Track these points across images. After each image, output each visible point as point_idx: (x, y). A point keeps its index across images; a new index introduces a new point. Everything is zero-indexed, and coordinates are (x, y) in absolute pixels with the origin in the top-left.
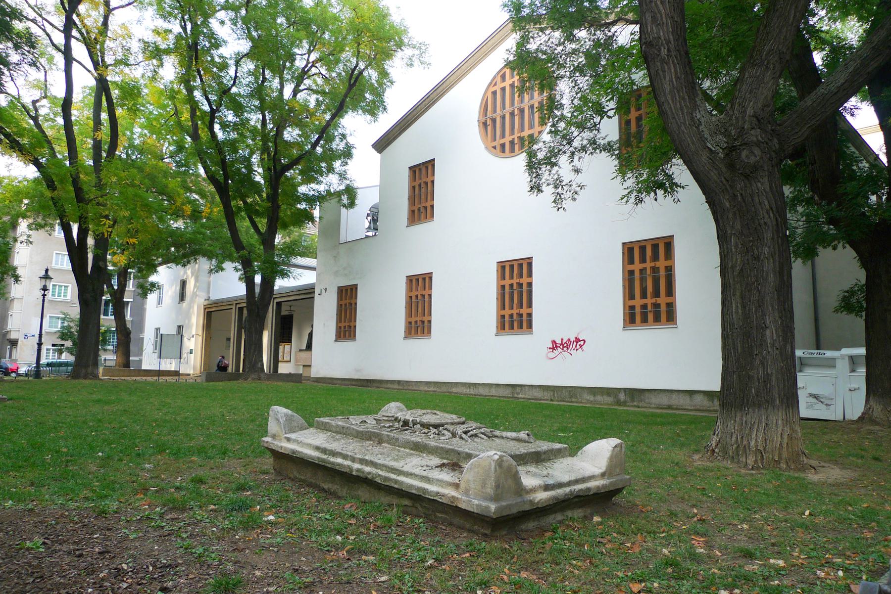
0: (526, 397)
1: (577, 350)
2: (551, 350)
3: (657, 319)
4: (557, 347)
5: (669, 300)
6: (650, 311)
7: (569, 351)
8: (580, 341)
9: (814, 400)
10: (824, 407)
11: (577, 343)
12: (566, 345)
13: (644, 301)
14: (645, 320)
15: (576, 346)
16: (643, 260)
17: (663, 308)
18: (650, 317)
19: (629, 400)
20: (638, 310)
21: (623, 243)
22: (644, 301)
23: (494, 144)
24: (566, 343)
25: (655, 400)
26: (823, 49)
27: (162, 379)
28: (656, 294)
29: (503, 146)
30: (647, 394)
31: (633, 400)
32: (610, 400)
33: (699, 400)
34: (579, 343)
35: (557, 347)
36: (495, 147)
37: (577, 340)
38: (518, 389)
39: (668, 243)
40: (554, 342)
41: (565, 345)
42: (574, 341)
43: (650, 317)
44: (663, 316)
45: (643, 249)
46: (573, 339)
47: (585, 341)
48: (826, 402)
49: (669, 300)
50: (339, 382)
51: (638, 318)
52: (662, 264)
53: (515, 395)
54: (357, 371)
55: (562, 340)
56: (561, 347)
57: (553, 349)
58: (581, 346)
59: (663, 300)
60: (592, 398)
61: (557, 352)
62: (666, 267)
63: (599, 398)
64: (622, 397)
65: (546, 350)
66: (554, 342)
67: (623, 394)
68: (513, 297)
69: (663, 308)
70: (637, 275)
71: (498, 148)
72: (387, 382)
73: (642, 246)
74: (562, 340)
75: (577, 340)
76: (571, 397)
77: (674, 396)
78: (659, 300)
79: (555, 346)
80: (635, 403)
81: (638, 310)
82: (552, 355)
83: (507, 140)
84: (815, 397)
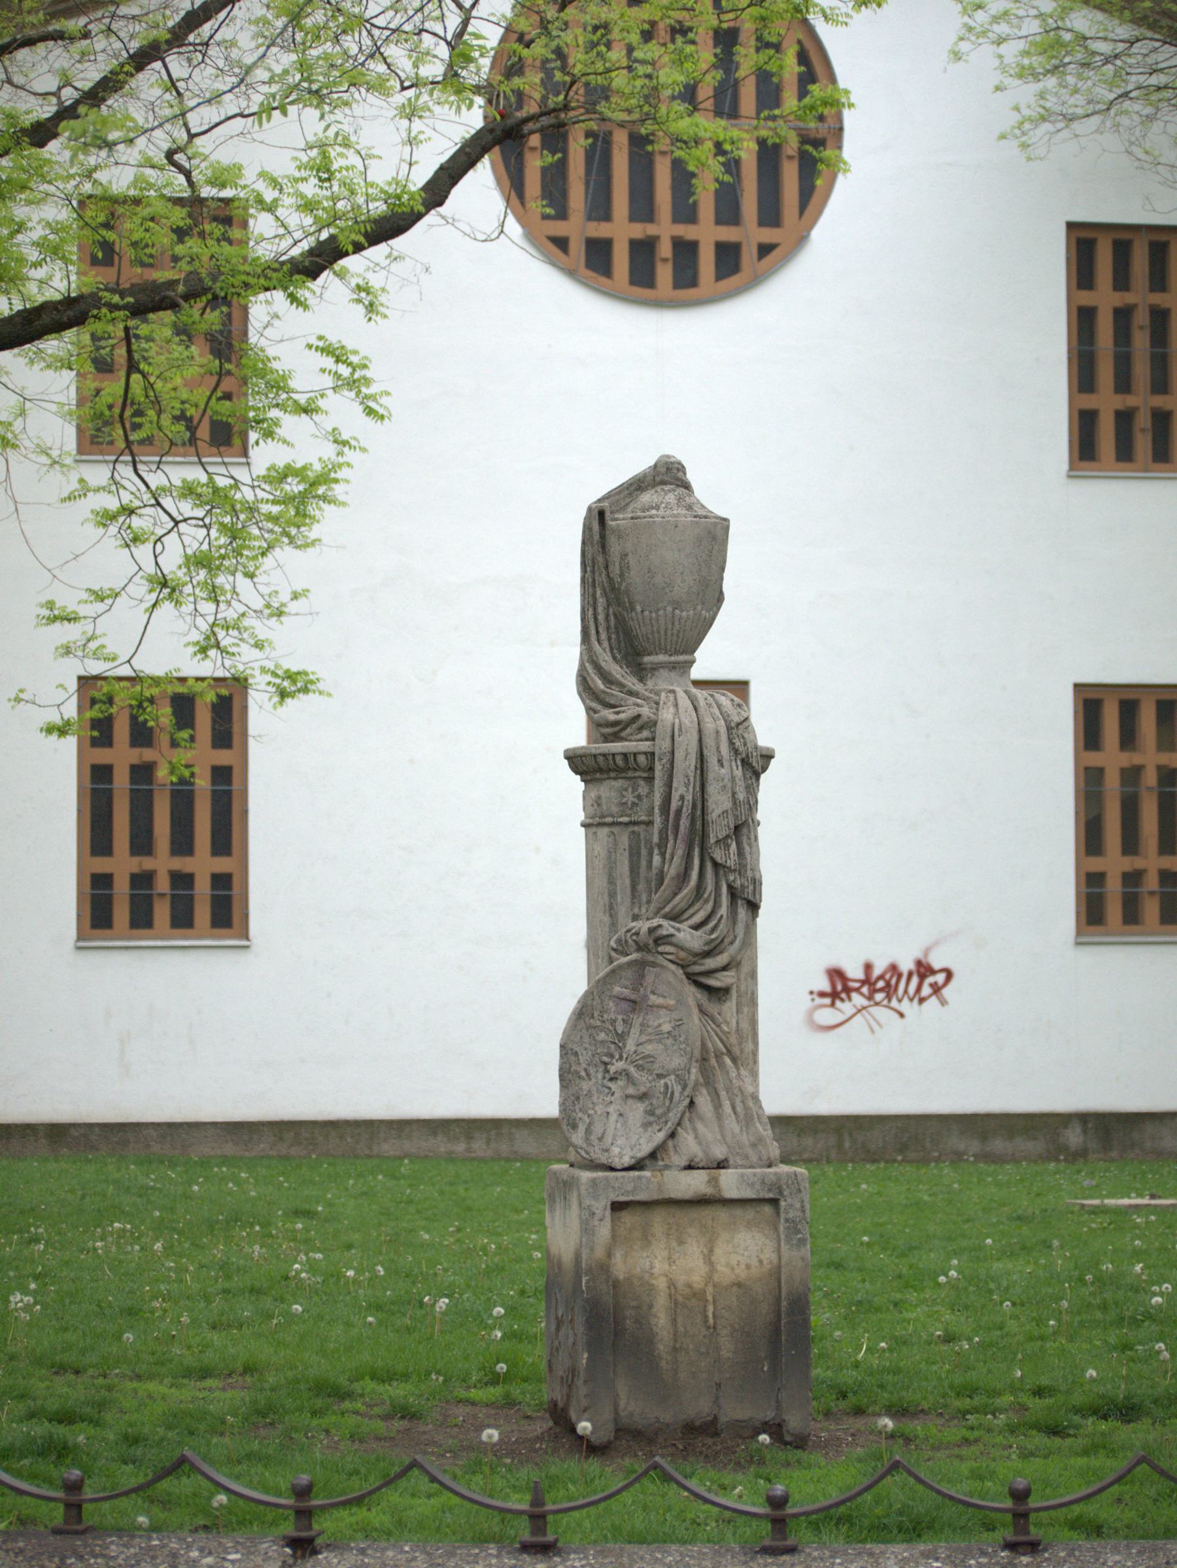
1: (922, 1000)
2: (827, 1001)
3: (183, 920)
4: (848, 990)
6: (1152, 893)
7: (894, 1003)
8: (933, 972)
11: (922, 977)
14: (142, 920)
15: (919, 989)
17: (203, 888)
18: (162, 912)
20: (122, 888)
21: (80, 678)
22: (181, 864)
23: (559, 228)
24: (881, 977)
26: (342, 267)
29: (643, 250)
34: (931, 980)
36: (562, 243)
37: (923, 969)
40: (836, 974)
41: (881, 984)
42: (910, 974)
43: (162, 912)
44: (203, 913)
46: (906, 965)
47: (949, 975)
49: (222, 865)
51: (121, 913)
56: (865, 990)
57: (834, 995)
58: (936, 989)
61: (846, 1008)
62: (134, 769)
65: (806, 1002)
66: (836, 974)
67: (1078, 1130)
69: (203, 888)
70: (121, 781)
71: (577, 248)
74: (868, 967)
75: (923, 969)
81: (122, 888)
82: (827, 1016)
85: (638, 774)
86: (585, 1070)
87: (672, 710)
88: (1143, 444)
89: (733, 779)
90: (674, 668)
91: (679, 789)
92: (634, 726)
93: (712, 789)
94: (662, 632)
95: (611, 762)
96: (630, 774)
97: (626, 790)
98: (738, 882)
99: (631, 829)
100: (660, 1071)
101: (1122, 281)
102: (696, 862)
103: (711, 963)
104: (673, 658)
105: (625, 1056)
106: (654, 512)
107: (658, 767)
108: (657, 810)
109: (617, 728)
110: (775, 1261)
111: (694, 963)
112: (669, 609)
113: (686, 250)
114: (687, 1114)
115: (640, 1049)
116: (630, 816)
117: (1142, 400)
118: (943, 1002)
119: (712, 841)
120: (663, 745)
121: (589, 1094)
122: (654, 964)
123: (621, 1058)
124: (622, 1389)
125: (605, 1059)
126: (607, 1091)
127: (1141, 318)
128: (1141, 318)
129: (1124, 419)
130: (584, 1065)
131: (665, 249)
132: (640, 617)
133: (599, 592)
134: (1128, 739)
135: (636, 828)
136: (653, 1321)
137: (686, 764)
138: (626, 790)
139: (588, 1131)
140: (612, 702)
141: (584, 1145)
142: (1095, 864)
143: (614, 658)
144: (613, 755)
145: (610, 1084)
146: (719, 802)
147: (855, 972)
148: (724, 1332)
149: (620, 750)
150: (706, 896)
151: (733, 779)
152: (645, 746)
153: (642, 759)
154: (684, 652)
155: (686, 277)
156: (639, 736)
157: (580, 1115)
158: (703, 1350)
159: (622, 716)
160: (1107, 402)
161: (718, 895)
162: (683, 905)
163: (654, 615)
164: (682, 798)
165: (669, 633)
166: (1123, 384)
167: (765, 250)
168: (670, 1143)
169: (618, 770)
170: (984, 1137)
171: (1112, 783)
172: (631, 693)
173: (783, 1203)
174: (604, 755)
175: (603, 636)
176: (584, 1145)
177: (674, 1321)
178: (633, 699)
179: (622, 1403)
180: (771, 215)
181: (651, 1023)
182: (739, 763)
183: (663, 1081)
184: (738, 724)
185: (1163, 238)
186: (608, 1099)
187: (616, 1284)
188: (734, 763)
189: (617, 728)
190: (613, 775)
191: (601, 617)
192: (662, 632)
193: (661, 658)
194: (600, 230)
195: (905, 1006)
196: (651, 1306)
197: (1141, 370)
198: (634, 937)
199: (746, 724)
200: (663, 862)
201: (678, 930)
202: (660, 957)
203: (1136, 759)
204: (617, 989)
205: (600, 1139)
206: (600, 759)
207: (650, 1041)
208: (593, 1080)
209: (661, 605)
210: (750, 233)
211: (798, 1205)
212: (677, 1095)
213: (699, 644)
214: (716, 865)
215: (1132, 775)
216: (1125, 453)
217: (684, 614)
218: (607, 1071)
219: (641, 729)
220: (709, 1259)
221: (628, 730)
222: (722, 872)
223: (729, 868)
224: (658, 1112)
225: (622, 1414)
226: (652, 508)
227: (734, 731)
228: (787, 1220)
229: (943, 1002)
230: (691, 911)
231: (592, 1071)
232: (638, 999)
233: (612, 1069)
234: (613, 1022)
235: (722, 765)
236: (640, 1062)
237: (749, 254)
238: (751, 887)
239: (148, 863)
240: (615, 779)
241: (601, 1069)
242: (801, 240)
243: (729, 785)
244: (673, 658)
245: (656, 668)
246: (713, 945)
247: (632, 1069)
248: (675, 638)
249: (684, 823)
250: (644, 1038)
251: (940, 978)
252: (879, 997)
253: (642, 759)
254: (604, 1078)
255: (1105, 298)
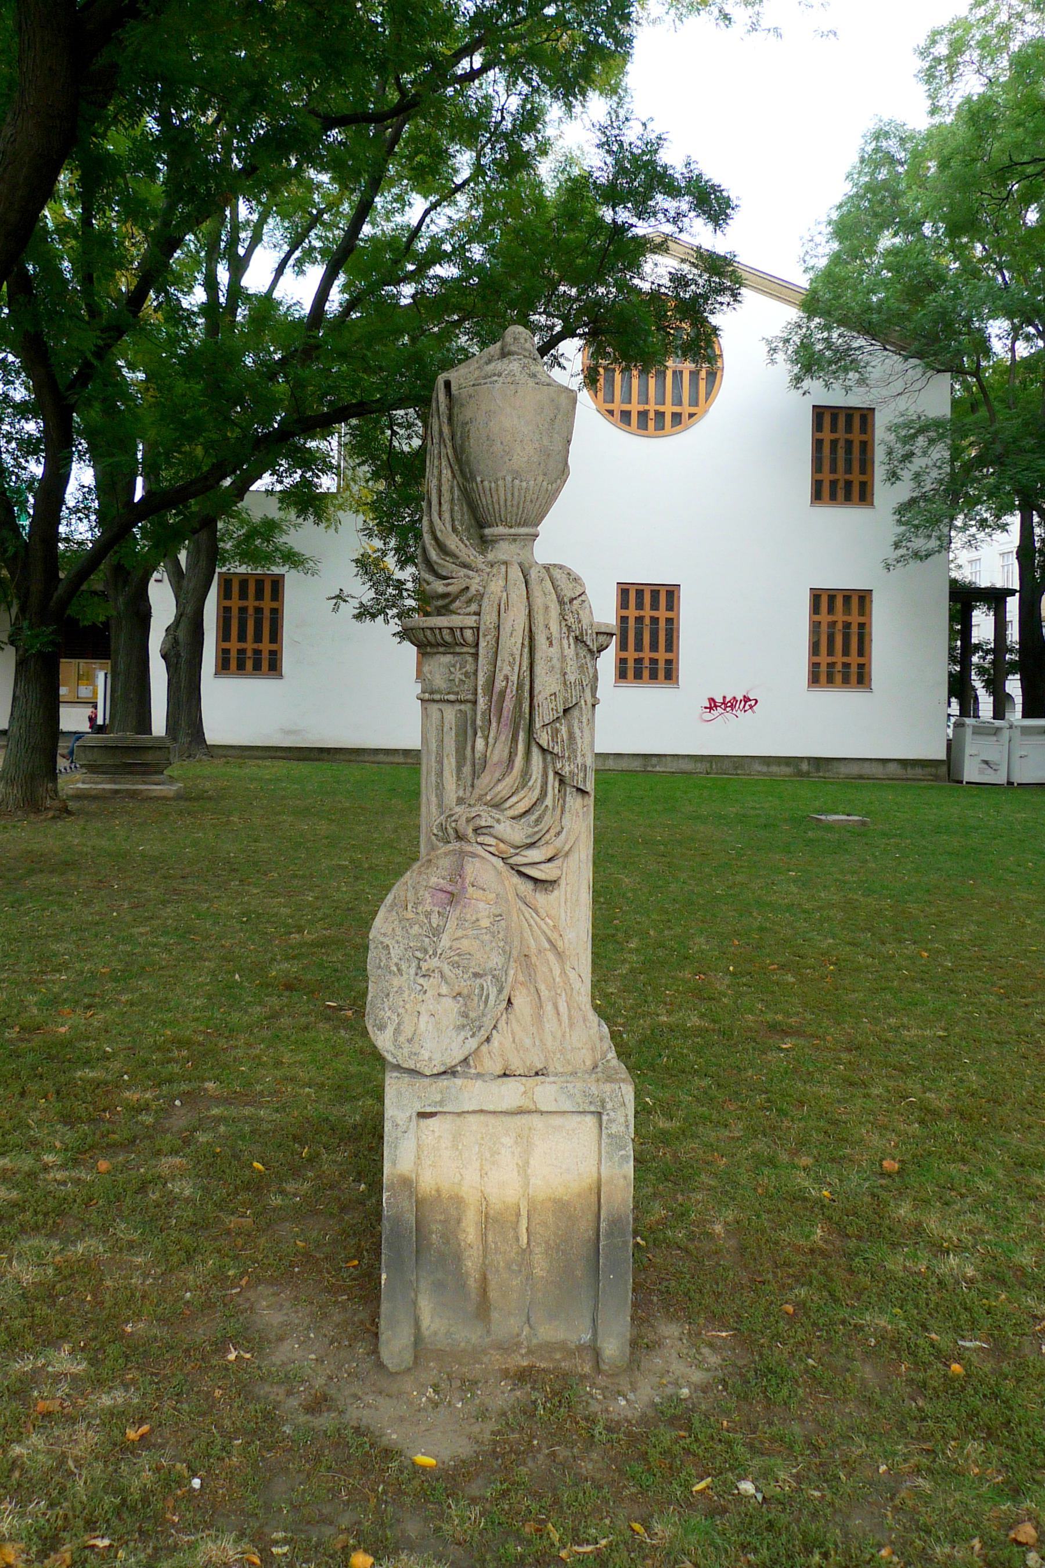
0: (668, 770)
4: (716, 706)
5: (273, 647)
9: (985, 766)
10: (993, 772)
11: (746, 702)
12: (729, 704)
13: (830, 659)
16: (640, 606)
18: (646, 673)
19: (812, 770)
23: (610, 406)
25: (844, 770)
27: (252, 768)
28: (654, 647)
30: (835, 764)
31: (818, 770)
32: (787, 770)
33: (892, 768)
35: (716, 706)
36: (611, 412)
37: (746, 699)
38: (654, 761)
39: (864, 598)
45: (640, 593)
46: (739, 697)
47: (757, 702)
48: (995, 767)
50: (221, 752)
52: (267, 604)
53: (649, 769)
54: (289, 732)
55: (724, 698)
57: (711, 708)
58: (751, 707)
59: (266, 646)
60: (765, 769)
61: (715, 713)
63: (774, 769)
64: (805, 767)
65: (700, 710)
66: (712, 700)
68: (627, 638)
71: (617, 414)
72: (376, 751)
73: (832, 595)
74: (724, 698)
75: (746, 699)
76: (736, 768)
77: (867, 765)
78: (261, 646)
79: (713, 704)
80: (821, 774)
83: (635, 407)
84: (986, 762)
85: (465, 650)
86: (397, 965)
87: (502, 583)
88: (841, 493)
89: (563, 658)
90: (515, 540)
91: (504, 669)
92: (463, 598)
93: (540, 669)
94: (502, 503)
95: (438, 637)
96: (458, 649)
97: (454, 666)
98: (567, 769)
99: (457, 707)
100: (477, 970)
101: (834, 429)
102: (521, 747)
103: (534, 855)
104: (513, 531)
105: (439, 952)
106: (495, 378)
107: (482, 644)
108: (480, 691)
109: (447, 601)
110: (595, 1175)
111: (517, 854)
112: (509, 478)
113: (660, 415)
114: (504, 1016)
115: (456, 945)
116: (457, 693)
117: (841, 476)
118: (754, 712)
119: (538, 726)
120: (489, 619)
121: (400, 991)
122: (474, 855)
123: (435, 954)
124: (426, 1306)
125: (419, 954)
126: (419, 988)
127: (841, 444)
128: (841, 444)
129: (834, 483)
130: (395, 960)
131: (652, 415)
132: (480, 488)
133: (444, 463)
134: (831, 610)
135: (463, 707)
136: (462, 1236)
137: (513, 642)
138: (454, 666)
139: (397, 1031)
140: (444, 574)
141: (392, 1048)
142: (816, 659)
143: (454, 530)
144: (440, 629)
145: (421, 981)
146: (547, 684)
147: (719, 700)
148: (537, 1250)
149: (446, 624)
150: (530, 784)
151: (563, 658)
152: (471, 621)
153: (468, 634)
154: (525, 524)
155: (660, 426)
156: (468, 610)
157: (389, 1014)
158: (515, 1267)
159: (450, 589)
160: (827, 477)
161: (545, 784)
162: (505, 793)
163: (493, 485)
164: (507, 678)
165: (509, 503)
166: (833, 470)
167: (691, 416)
168: (484, 1048)
169: (446, 644)
170: (768, 765)
171: (824, 628)
172: (465, 566)
173: (605, 1118)
174: (431, 629)
175: (446, 507)
176: (392, 1048)
177: (484, 1236)
178: (464, 571)
179: (426, 1322)
180: (694, 402)
181: (468, 916)
182: (572, 641)
183: (478, 981)
184: (572, 600)
185: (851, 412)
186: (420, 998)
187: (419, 1203)
188: (565, 642)
189: (447, 601)
190: (441, 649)
191: (445, 488)
192: (502, 503)
193: (501, 530)
194: (626, 407)
195: (738, 713)
196: (459, 1221)
197: (841, 465)
198: (453, 825)
199: (583, 598)
200: (487, 744)
201: (498, 821)
202: (479, 847)
203: (834, 618)
204: (434, 880)
205: (410, 1041)
206: (445, 632)
207: (466, 936)
208: (405, 976)
209: (500, 475)
210: (686, 409)
211: (622, 1120)
212: (492, 998)
213: (543, 517)
214: (543, 750)
215: (832, 625)
216: (833, 497)
217: (524, 484)
218: (419, 968)
219: (469, 601)
220: (524, 1168)
221: (457, 603)
222: (549, 757)
223: (557, 755)
224: (472, 1015)
225: (426, 1333)
226: (494, 375)
227: (567, 607)
228: (609, 1136)
229: (754, 712)
230: (514, 799)
231: (404, 966)
232: (455, 891)
233: (424, 966)
234: (428, 915)
235: (551, 644)
236: (456, 958)
237: (685, 416)
238: (581, 775)
239: (642, 613)
240: (444, 654)
241: (414, 964)
242: (706, 411)
243: (558, 665)
244: (513, 531)
245: (501, 538)
246: (537, 837)
247: (446, 968)
248: (515, 508)
249: (509, 704)
250: (460, 933)
251: (753, 703)
252: (728, 709)
253: (468, 634)
254: (417, 974)
255: (827, 436)
